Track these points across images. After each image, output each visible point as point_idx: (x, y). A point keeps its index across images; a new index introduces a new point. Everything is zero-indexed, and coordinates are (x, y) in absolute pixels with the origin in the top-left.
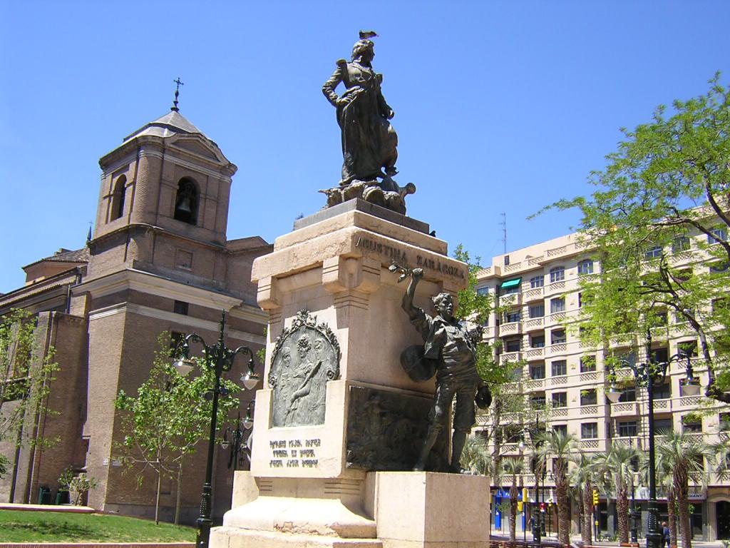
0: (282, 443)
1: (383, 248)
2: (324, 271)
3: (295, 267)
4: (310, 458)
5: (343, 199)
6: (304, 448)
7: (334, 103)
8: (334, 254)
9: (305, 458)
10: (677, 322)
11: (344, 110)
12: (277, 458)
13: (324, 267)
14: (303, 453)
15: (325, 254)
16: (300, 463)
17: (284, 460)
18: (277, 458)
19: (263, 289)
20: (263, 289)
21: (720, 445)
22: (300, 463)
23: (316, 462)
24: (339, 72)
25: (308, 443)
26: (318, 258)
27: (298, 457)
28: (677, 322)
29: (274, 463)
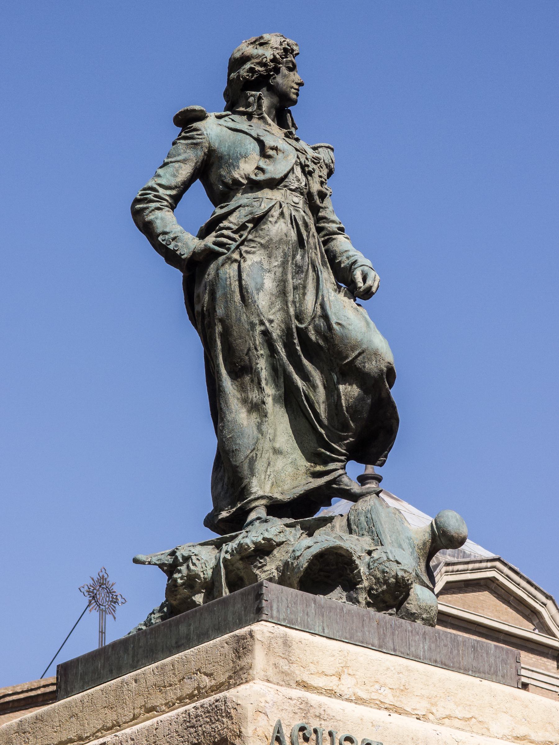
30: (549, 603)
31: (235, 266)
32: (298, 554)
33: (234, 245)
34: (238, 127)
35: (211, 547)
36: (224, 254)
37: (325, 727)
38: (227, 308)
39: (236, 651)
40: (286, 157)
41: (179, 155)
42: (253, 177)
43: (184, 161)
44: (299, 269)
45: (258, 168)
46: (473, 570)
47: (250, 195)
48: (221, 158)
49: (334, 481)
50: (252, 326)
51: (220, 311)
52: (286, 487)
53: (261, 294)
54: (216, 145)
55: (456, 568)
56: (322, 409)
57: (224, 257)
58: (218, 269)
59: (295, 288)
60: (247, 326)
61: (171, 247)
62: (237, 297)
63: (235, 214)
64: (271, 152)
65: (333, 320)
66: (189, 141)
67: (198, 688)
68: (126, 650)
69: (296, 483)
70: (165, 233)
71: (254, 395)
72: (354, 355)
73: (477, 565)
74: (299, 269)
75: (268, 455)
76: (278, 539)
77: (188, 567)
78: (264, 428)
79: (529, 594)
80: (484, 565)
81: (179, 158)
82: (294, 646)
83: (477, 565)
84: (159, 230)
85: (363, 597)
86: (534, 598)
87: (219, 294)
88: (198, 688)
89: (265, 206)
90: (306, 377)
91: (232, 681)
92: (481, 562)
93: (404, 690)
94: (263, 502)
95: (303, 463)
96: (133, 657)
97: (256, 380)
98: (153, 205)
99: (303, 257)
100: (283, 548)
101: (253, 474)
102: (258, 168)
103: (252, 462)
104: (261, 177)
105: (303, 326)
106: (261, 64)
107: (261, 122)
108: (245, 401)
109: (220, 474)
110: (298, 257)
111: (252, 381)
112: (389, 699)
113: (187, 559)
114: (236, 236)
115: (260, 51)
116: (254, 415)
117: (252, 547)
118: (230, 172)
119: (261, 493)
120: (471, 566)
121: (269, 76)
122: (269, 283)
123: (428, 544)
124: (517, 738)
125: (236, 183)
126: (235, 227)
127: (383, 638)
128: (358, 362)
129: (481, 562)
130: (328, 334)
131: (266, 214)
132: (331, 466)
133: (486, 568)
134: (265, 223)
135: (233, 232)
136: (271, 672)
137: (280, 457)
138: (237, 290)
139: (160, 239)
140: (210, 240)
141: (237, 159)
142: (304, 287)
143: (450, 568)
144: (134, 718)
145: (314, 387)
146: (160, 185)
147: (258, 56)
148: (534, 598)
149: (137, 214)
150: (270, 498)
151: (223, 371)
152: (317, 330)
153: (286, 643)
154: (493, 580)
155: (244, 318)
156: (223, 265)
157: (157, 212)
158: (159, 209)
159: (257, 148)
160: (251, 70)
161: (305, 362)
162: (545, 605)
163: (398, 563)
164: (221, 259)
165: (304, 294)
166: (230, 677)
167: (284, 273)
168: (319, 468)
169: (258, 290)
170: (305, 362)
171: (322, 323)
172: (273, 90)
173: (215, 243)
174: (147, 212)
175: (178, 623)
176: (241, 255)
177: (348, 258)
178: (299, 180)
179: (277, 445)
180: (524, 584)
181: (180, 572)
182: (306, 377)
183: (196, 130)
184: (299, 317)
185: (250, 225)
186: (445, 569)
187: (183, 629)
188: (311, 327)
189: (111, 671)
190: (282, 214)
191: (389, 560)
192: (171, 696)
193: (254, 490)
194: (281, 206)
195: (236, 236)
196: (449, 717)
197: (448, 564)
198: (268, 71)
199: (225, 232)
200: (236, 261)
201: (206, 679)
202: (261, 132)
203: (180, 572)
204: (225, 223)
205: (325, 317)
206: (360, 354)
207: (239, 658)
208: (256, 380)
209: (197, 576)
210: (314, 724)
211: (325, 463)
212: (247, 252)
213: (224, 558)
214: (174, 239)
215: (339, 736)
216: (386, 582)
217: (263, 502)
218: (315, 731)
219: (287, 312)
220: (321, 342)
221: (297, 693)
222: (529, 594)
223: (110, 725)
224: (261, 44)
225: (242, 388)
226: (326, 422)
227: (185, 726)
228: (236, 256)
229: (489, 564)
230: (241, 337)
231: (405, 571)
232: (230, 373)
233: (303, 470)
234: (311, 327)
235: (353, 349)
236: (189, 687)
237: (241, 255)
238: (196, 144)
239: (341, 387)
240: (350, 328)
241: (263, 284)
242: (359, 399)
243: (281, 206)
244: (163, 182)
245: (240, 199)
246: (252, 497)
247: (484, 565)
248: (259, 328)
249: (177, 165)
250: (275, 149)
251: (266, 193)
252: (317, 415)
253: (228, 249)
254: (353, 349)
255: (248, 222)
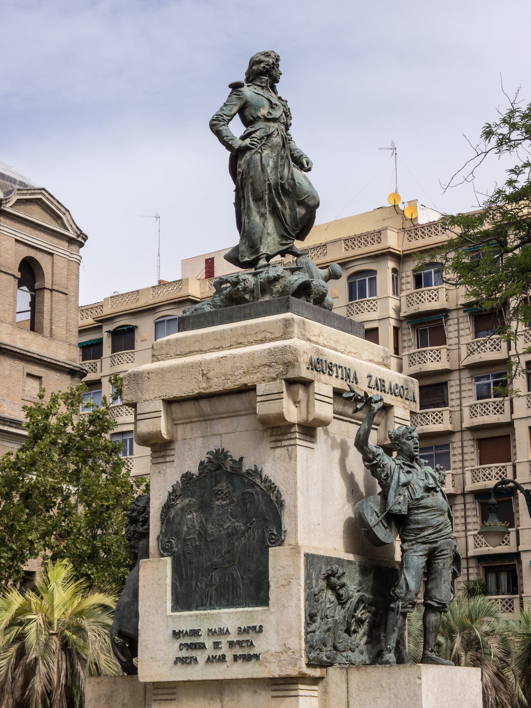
0: (195, 633)
1: (334, 369)
2: (259, 399)
3: (204, 388)
4: (246, 651)
5: (83, 241)
6: (234, 637)
7: (228, 146)
8: (274, 375)
9: (239, 652)
10: (420, 409)
11: (287, 187)
12: (184, 653)
13: (258, 393)
14: (202, 646)
15: (259, 375)
16: (229, 658)
17: (201, 656)
18: (184, 653)
19: (263, 398)
20: (263, 398)
21: (85, 661)
22: (229, 658)
23: (257, 657)
24: (459, 226)
25: (241, 631)
26: (247, 380)
27: (224, 649)
28: (420, 409)
29: (181, 661)
30: (67, 213)
31: (259, 155)
32: (292, 282)
33: (259, 146)
34: (259, 92)
35: (251, 275)
36: (254, 149)
37: (324, 358)
38: (255, 172)
39: (285, 325)
40: (279, 109)
41: (233, 102)
42: (266, 116)
43: (235, 105)
44: (282, 158)
45: (269, 112)
46: (31, 194)
47: (264, 123)
48: (251, 106)
49: (290, 248)
50: (265, 181)
51: (252, 173)
52: (271, 249)
54: (249, 100)
55: (23, 192)
56: (288, 218)
57: (255, 150)
58: (252, 155)
59: (281, 165)
60: (263, 181)
61: (230, 143)
62: (260, 168)
63: (258, 132)
64: (274, 106)
65: (297, 181)
66: (238, 96)
67: (265, 338)
68: (216, 315)
69: (275, 248)
70: (227, 136)
71: (263, 210)
72: (305, 197)
73: (33, 191)
74: (282, 158)
75: (266, 235)
76: (282, 275)
77: (245, 283)
78: (265, 224)
79: (58, 208)
80: (36, 191)
81: (233, 103)
82: (306, 324)
83: (33, 191)
84: (224, 135)
85: (312, 301)
86: (60, 210)
87: (252, 166)
88: (265, 338)
89: (272, 130)
90: (282, 203)
91: (283, 337)
92: (35, 190)
93: (337, 342)
94: (265, 256)
95: (277, 239)
96: (220, 318)
97: (264, 204)
98: (222, 123)
99: (284, 153)
100: (283, 279)
101: (261, 244)
102: (269, 112)
103: (261, 238)
104: (270, 117)
105: (283, 182)
106: (268, 65)
107: (267, 91)
108: (259, 212)
109: (244, 241)
110: (282, 152)
111: (262, 204)
112: (333, 346)
113: (244, 280)
114: (259, 141)
115: (267, 59)
116: (262, 218)
117: (273, 278)
118: (256, 112)
119: (264, 252)
120: (30, 192)
121: (270, 70)
122: (271, 163)
124: (370, 360)
125: (259, 117)
126: (259, 138)
127: (324, 320)
128: (306, 201)
129: (35, 190)
130: (294, 187)
131: (272, 133)
132: (289, 242)
133: (37, 193)
134: (271, 137)
135: (258, 140)
136: (300, 335)
138: (260, 165)
139: (225, 138)
140: (248, 141)
141: (260, 108)
142: (284, 166)
143: (20, 192)
144: (230, 346)
145: (285, 208)
146: (224, 114)
147: (267, 61)
148: (60, 210)
149: (213, 126)
150: (267, 254)
151: (251, 199)
152: (289, 184)
153: (304, 323)
154: (40, 199)
155: (262, 177)
156: (254, 154)
157: (223, 126)
158: (224, 125)
159: (268, 103)
160: (264, 67)
161: (282, 197)
162: (65, 214)
163: (324, 287)
164: (253, 151)
165: (284, 168)
166: (282, 335)
167: (277, 159)
168: (284, 242)
170: (282, 197)
171: (291, 182)
172: (271, 76)
173: (250, 144)
174: (219, 126)
175: (244, 308)
176: (262, 150)
177: (298, 153)
178: (284, 119)
180: (55, 203)
181: (241, 285)
182: (282, 203)
183: (240, 92)
184: (282, 178)
185: (266, 138)
186: (17, 192)
187: (247, 311)
188: (286, 183)
189: (208, 323)
190: (278, 134)
191: (320, 285)
192: (251, 339)
193: (261, 250)
194: (278, 130)
195: (259, 141)
196: (350, 352)
197: (18, 190)
198: (270, 68)
199: (255, 139)
200: (259, 153)
201: (269, 335)
202: (269, 97)
203: (241, 285)
204: (253, 135)
205: (293, 179)
206: (307, 197)
207: (287, 328)
208: (264, 204)
209: (248, 287)
210: (321, 358)
211: (287, 240)
212: (264, 149)
213: (260, 282)
214: (231, 139)
215: (328, 362)
216: (318, 294)
217: (265, 256)
218: (321, 360)
219: (277, 176)
220: (290, 190)
221: (315, 345)
222: (58, 208)
223: (217, 347)
224: (267, 56)
225: (258, 207)
226: (289, 224)
227: (268, 354)
228: (260, 151)
229: (39, 191)
230: (260, 186)
232: (253, 200)
233: (277, 242)
234: (286, 183)
235: (305, 194)
236: (260, 337)
237: (262, 150)
238: (241, 98)
239: (298, 210)
240: (304, 185)
242: (305, 216)
243: (278, 130)
244: (226, 113)
245: (261, 124)
246: (261, 253)
247: (36, 191)
248: (268, 182)
249: (232, 106)
250: (276, 105)
251: (272, 124)
252: (285, 220)
253: (256, 147)
254: (305, 194)
255: (265, 136)
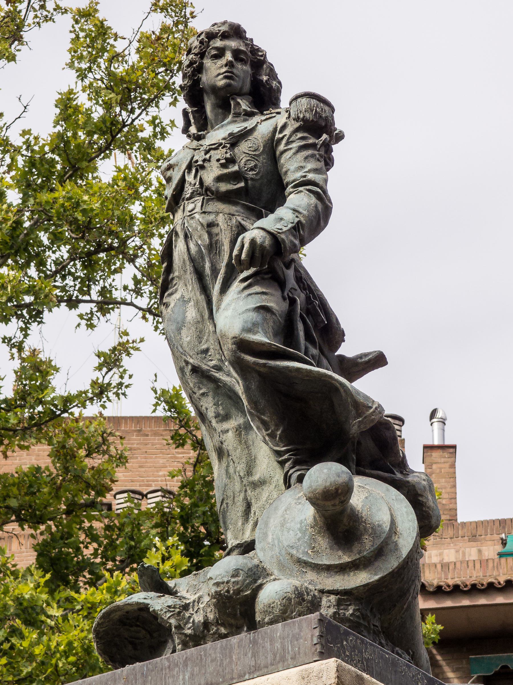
53: (184, 332)
123: (317, 516)
137: (265, 488)
169: (179, 330)
179: (256, 477)
231: (217, 584)
241: (185, 318)
